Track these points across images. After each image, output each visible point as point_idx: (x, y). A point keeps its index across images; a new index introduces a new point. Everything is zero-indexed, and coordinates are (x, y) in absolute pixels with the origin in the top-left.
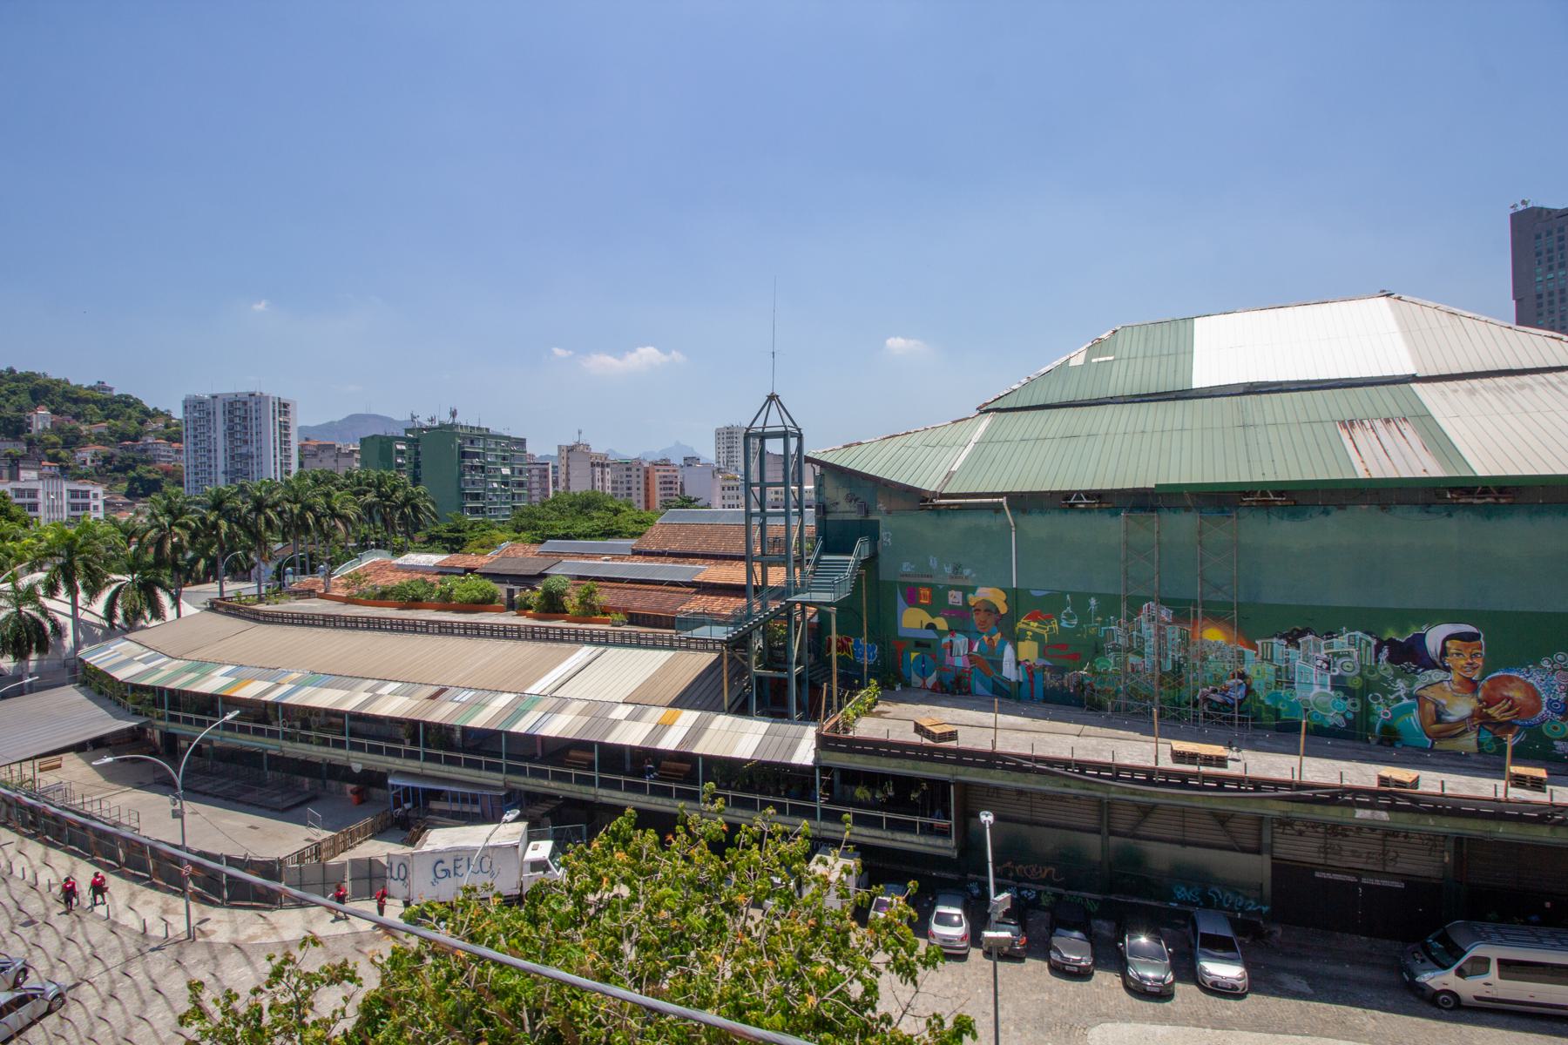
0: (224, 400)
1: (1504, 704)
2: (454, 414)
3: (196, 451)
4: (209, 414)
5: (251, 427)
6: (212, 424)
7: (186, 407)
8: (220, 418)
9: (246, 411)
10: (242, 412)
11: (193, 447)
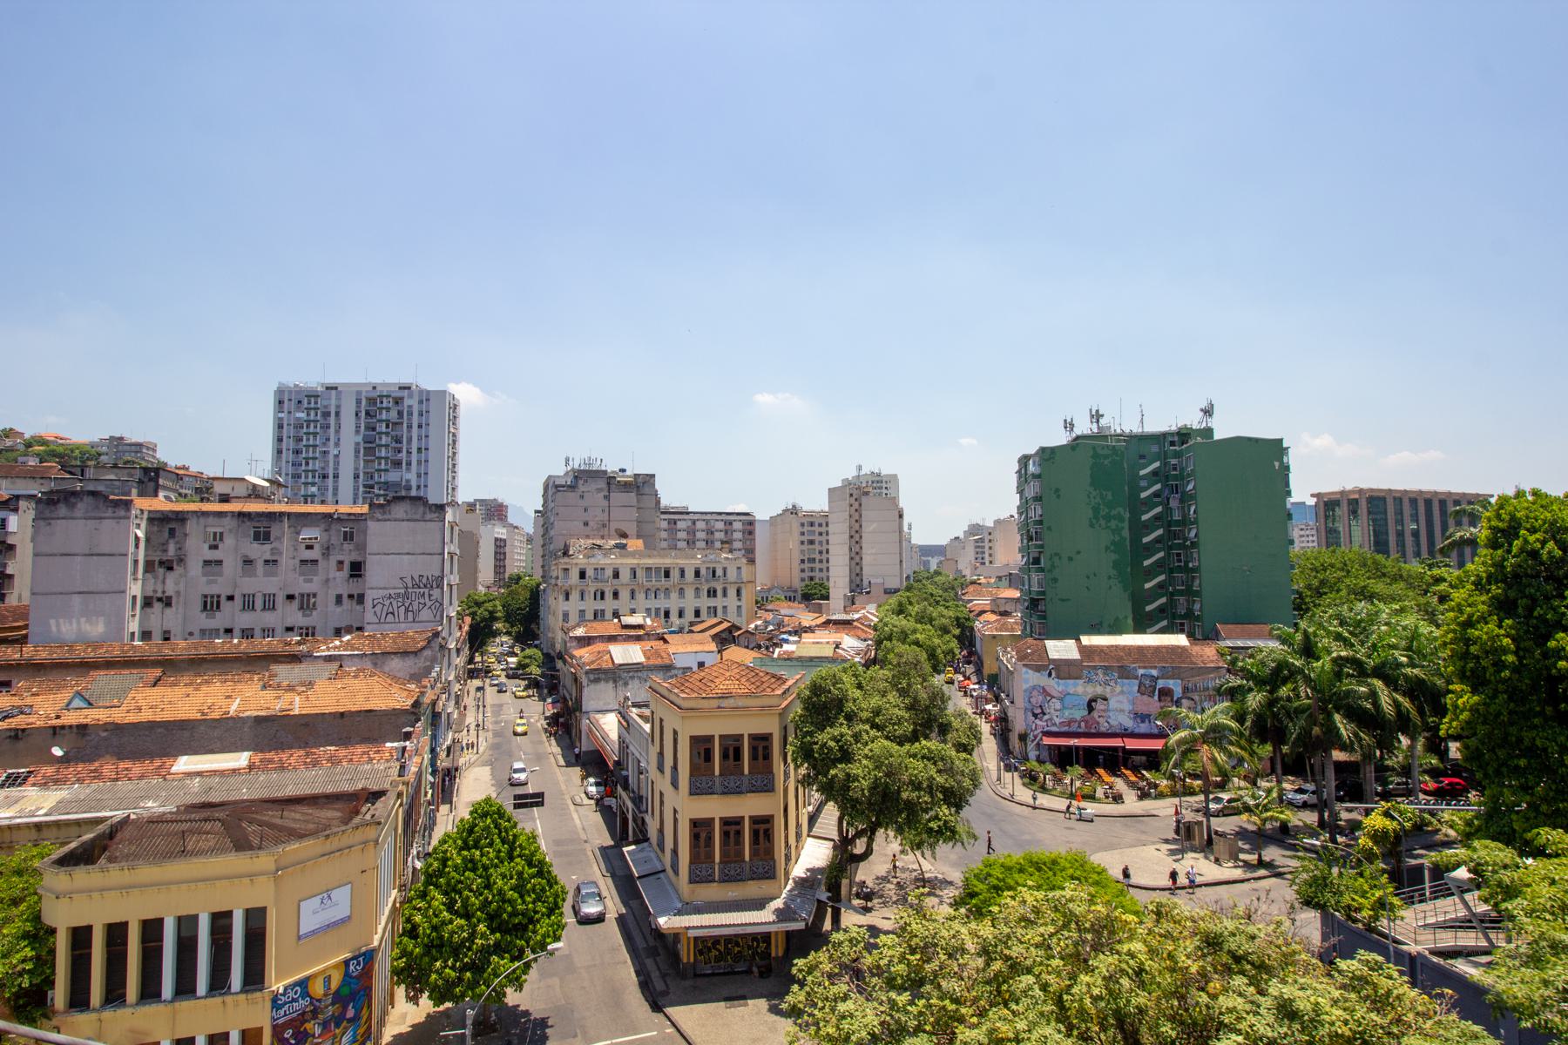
0: (359, 393)
4: (326, 415)
5: (410, 440)
6: (332, 430)
9: (400, 414)
10: (393, 415)
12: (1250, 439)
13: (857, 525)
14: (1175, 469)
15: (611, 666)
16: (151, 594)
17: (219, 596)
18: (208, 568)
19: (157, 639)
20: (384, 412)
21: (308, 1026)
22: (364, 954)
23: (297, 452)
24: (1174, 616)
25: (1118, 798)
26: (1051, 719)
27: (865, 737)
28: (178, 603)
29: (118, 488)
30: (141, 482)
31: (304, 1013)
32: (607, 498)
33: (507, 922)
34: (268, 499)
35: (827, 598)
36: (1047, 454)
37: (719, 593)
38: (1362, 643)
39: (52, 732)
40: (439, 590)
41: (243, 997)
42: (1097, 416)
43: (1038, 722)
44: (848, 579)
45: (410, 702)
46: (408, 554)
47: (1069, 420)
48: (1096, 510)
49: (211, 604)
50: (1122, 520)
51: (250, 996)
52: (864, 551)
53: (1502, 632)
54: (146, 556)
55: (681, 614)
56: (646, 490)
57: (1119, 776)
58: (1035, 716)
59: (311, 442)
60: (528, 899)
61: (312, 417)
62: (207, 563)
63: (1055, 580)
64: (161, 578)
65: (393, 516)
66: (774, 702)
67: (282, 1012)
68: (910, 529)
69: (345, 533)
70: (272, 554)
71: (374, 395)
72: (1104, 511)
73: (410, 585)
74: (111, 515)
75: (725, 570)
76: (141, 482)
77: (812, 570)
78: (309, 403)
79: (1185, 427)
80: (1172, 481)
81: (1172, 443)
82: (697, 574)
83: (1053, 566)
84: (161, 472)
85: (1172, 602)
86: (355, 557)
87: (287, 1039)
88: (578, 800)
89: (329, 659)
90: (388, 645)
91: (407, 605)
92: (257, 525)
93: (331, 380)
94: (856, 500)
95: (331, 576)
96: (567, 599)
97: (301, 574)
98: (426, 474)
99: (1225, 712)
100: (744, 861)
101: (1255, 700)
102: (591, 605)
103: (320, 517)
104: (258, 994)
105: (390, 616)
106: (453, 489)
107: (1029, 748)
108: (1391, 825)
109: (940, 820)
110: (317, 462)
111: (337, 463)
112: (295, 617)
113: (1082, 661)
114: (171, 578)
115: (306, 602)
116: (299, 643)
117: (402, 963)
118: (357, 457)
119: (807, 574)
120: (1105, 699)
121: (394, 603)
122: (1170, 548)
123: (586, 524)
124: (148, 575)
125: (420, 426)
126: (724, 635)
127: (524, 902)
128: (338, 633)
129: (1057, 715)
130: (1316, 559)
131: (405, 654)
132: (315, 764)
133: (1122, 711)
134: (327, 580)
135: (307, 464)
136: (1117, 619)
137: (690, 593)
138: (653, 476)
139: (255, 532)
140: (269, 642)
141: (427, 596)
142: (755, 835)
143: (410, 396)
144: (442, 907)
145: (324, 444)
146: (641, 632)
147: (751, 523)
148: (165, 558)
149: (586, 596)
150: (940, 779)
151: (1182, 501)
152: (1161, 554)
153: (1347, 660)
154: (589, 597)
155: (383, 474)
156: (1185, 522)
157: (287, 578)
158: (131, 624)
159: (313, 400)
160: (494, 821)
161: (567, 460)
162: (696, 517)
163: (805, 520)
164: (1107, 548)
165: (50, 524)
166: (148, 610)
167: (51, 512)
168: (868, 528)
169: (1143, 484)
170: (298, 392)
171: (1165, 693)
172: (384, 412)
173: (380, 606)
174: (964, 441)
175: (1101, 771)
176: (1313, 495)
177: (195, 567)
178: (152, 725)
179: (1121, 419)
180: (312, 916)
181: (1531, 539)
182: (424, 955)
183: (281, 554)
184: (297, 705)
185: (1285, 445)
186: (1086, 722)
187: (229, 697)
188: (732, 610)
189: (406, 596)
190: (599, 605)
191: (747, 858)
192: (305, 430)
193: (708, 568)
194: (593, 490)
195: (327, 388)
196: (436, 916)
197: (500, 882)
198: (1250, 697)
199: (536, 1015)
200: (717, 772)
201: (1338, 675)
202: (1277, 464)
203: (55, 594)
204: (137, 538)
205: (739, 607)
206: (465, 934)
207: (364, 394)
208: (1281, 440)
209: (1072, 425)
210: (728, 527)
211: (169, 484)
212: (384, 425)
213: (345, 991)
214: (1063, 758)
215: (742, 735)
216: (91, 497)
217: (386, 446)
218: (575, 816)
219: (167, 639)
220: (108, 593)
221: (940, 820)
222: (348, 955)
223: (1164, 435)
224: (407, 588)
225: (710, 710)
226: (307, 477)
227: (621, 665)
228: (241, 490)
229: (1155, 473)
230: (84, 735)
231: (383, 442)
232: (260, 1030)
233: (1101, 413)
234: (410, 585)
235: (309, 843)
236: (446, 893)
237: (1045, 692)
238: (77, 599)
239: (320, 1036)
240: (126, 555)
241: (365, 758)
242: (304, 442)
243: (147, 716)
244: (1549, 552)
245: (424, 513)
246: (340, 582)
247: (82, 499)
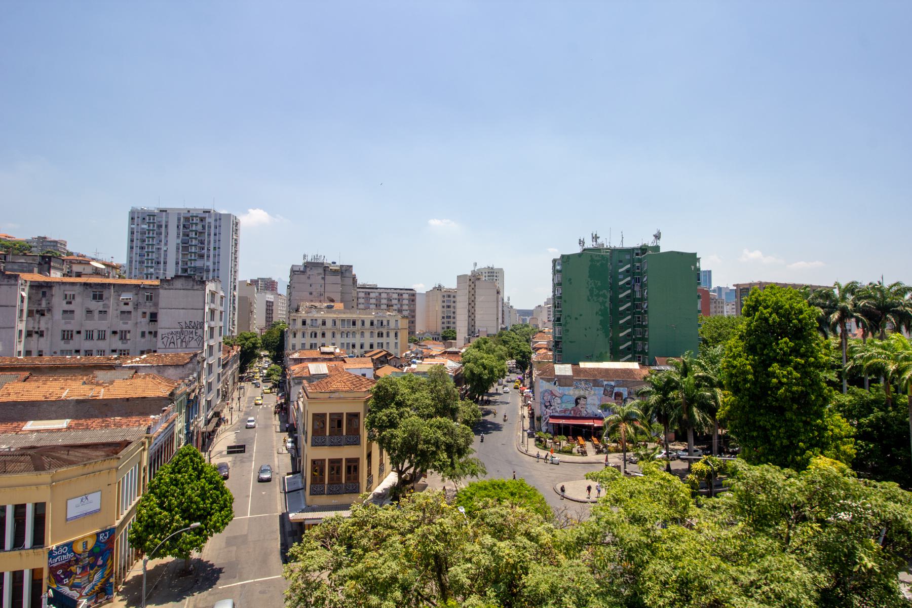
0: (179, 214)
3: (142, 262)
4: (160, 226)
5: (209, 243)
6: (163, 236)
7: (133, 219)
8: (173, 230)
9: (204, 227)
10: (199, 228)
11: (138, 259)
12: (678, 253)
13: (473, 297)
14: (638, 269)
15: (308, 375)
16: (31, 329)
17: (72, 331)
18: (66, 315)
19: (35, 355)
21: (73, 568)
22: (109, 530)
23: (142, 248)
24: (635, 352)
25: (584, 453)
26: (555, 409)
27: (407, 415)
28: (47, 335)
30: (40, 264)
31: (70, 561)
32: (324, 278)
33: (194, 514)
34: (104, 276)
35: (455, 339)
36: (565, 259)
37: (385, 335)
38: (712, 369)
41: (31, 551)
42: (595, 238)
43: (547, 410)
44: (467, 328)
45: (168, 393)
48: (591, 291)
49: (67, 336)
50: (605, 297)
51: (35, 551)
52: (476, 312)
53: (748, 362)
54: (29, 307)
55: (362, 347)
56: (347, 274)
57: (590, 441)
58: (546, 407)
59: (151, 243)
60: (207, 501)
61: (151, 228)
62: (65, 312)
63: (567, 331)
64: (37, 320)
65: (175, 287)
66: (362, 395)
67: (56, 560)
68: (509, 300)
69: (147, 296)
70: (104, 307)
71: (188, 215)
72: (596, 292)
73: (184, 327)
75: (388, 321)
76: (40, 264)
77: (449, 322)
78: (150, 219)
79: (645, 245)
80: (636, 275)
81: (637, 254)
82: (372, 324)
84: (52, 259)
85: (634, 344)
86: (153, 310)
87: (59, 575)
88: (280, 451)
89: (131, 368)
90: (168, 361)
93: (163, 206)
95: (138, 321)
96: (295, 337)
97: (122, 319)
98: (218, 262)
99: (638, 405)
100: (341, 483)
101: (653, 399)
102: (308, 341)
104: (40, 550)
106: (235, 272)
107: (542, 425)
108: (705, 468)
109: (441, 461)
111: (166, 255)
112: (119, 345)
113: (573, 376)
114: (43, 320)
115: (123, 336)
116: (116, 359)
117: (134, 536)
119: (446, 325)
120: (585, 398)
122: (634, 314)
123: (311, 294)
124: (30, 318)
125: (215, 235)
126: (382, 359)
127: (204, 503)
128: (142, 353)
129: (558, 407)
130: (718, 322)
131: (177, 366)
132: (107, 426)
133: (594, 405)
134: (137, 323)
135: (148, 255)
137: (367, 334)
138: (351, 266)
140: (98, 358)
142: (349, 469)
143: (210, 217)
144: (155, 505)
145: (158, 244)
146: (332, 356)
147: (414, 295)
148: (39, 309)
149: (306, 335)
150: (443, 439)
151: (641, 287)
152: (629, 317)
153: (702, 377)
154: (308, 335)
156: (642, 299)
157: (113, 321)
158: (18, 346)
159: (152, 218)
160: (191, 459)
161: (304, 256)
162: (381, 291)
163: (445, 294)
164: (597, 313)
166: (29, 338)
168: (479, 299)
169: (621, 277)
170: (143, 213)
171: (618, 395)
173: (165, 340)
175: (580, 438)
176: (734, 285)
177: (58, 314)
178: (15, 404)
179: (611, 240)
180: (75, 508)
181: (765, 311)
182: (144, 531)
183: (109, 307)
184: (102, 393)
185: (698, 257)
186: (574, 411)
187: (62, 388)
188: (392, 345)
189: (182, 333)
190: (314, 341)
191: (343, 481)
194: (315, 273)
196: (151, 510)
197: (189, 492)
198: (652, 397)
199: (216, 566)
200: (328, 434)
201: (698, 386)
202: (693, 267)
204: (22, 297)
205: (396, 343)
206: (168, 520)
208: (695, 254)
210: (400, 297)
211: (58, 265)
212: (194, 233)
213: (97, 550)
214: (560, 430)
215: (342, 414)
217: (195, 246)
218: (276, 460)
219: (41, 355)
221: (441, 461)
222: (98, 530)
223: (633, 249)
225: (324, 399)
226: (148, 263)
228: (88, 270)
229: (627, 271)
231: (193, 243)
232: (42, 569)
234: (184, 327)
235: (71, 468)
236: (159, 498)
237: (552, 393)
239: (80, 574)
240: (15, 306)
241: (137, 424)
242: (147, 242)
243: (13, 398)
244: (773, 319)
245: (193, 285)
246: (144, 324)
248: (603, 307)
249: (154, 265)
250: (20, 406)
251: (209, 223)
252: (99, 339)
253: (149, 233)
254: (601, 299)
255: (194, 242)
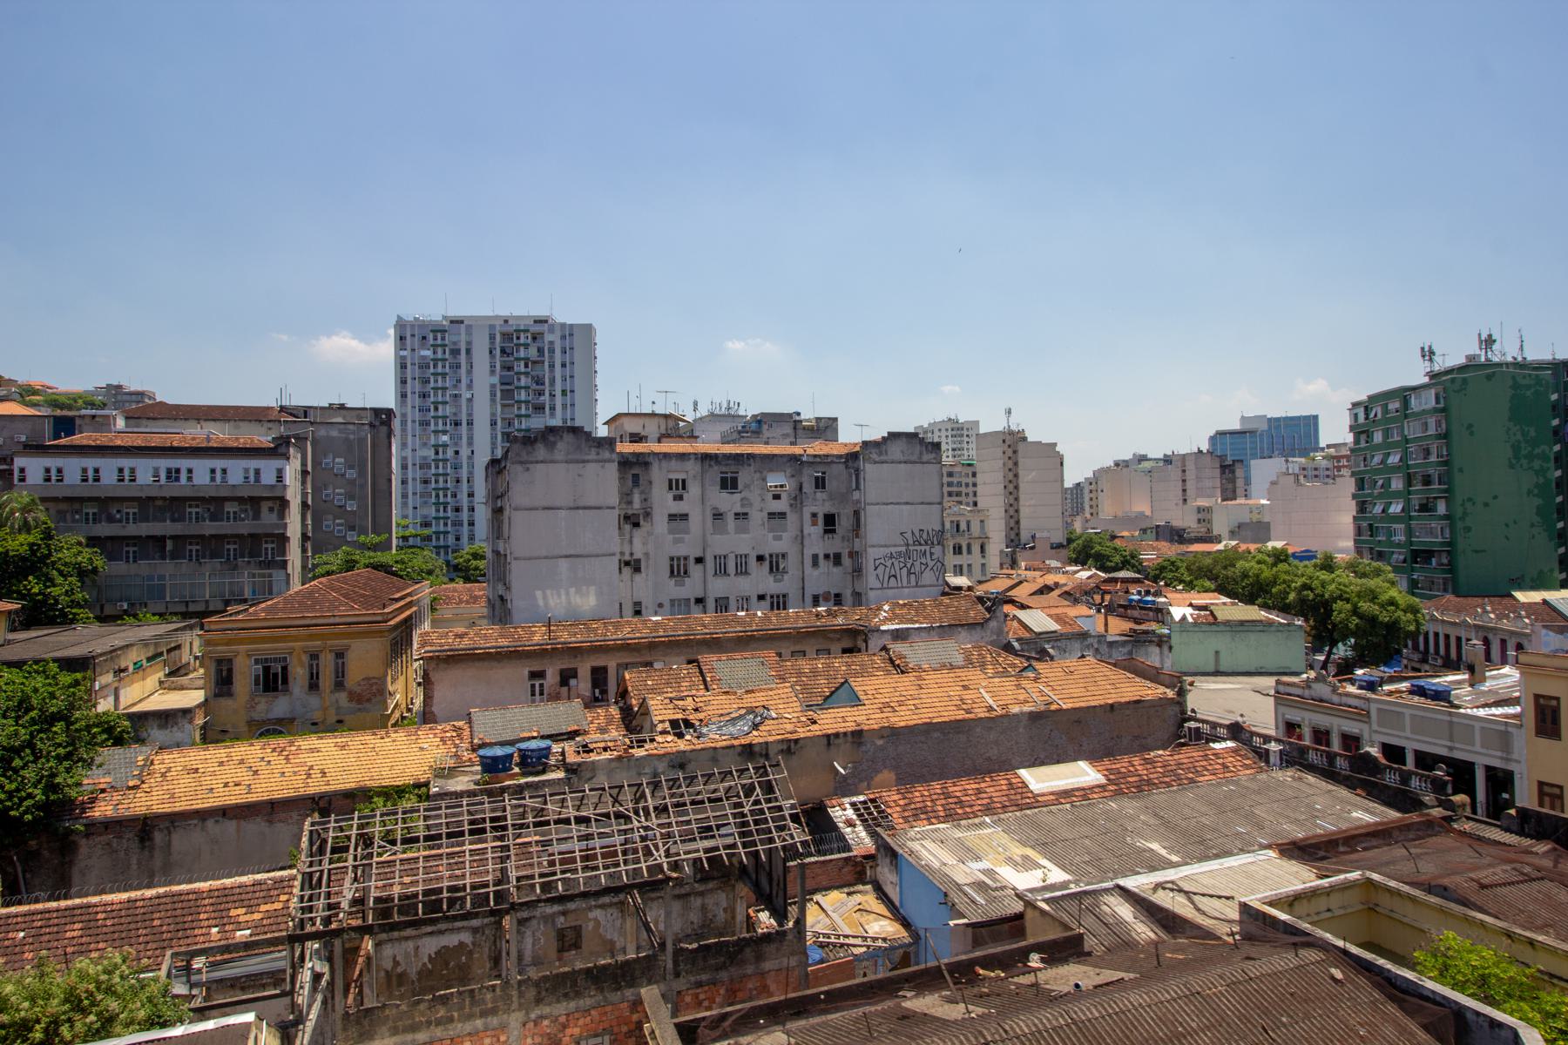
0: (492, 327)
1: (1160, 756)
2: (1428, 354)
10: (533, 352)
18: (674, 524)
20: (522, 349)
23: (424, 396)
28: (647, 567)
29: (354, 433)
30: (371, 425)
39: (826, 742)
40: (940, 547)
46: (907, 503)
47: (1426, 349)
48: (1516, 449)
52: (1021, 503)
59: (440, 384)
61: (440, 355)
64: (628, 537)
69: (817, 478)
70: (742, 506)
73: (911, 542)
74: (595, 457)
75: (968, 523)
78: (435, 339)
83: (1465, 514)
91: (909, 565)
92: (724, 469)
94: (1009, 446)
97: (771, 530)
103: (785, 460)
105: (892, 579)
110: (448, 406)
112: (770, 585)
114: (638, 535)
115: (774, 564)
118: (493, 400)
121: (896, 563)
125: (564, 365)
135: (436, 409)
136: (1541, 572)
138: (835, 420)
139: (722, 478)
141: (928, 554)
145: (455, 386)
148: (630, 512)
155: (523, 420)
159: (439, 335)
164: (1529, 492)
165: (528, 469)
167: (528, 453)
172: (522, 349)
173: (881, 568)
174: (947, 389)
189: (908, 555)
192: (432, 370)
193: (952, 522)
195: (452, 322)
203: (539, 558)
207: (498, 328)
209: (1432, 353)
212: (522, 363)
216: (571, 435)
217: (526, 388)
220: (597, 556)
224: (908, 545)
227: (1041, 633)
228: (652, 429)
230: (860, 744)
231: (523, 383)
233: (1494, 338)
234: (911, 542)
238: (563, 565)
245: (921, 453)
247: (561, 437)
248: (1541, 480)
249: (448, 427)
250: (936, 735)
251: (551, 343)
252: (737, 574)
253: (435, 366)
254: (1537, 464)
255: (523, 381)
